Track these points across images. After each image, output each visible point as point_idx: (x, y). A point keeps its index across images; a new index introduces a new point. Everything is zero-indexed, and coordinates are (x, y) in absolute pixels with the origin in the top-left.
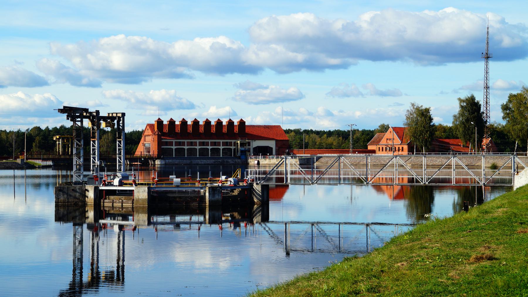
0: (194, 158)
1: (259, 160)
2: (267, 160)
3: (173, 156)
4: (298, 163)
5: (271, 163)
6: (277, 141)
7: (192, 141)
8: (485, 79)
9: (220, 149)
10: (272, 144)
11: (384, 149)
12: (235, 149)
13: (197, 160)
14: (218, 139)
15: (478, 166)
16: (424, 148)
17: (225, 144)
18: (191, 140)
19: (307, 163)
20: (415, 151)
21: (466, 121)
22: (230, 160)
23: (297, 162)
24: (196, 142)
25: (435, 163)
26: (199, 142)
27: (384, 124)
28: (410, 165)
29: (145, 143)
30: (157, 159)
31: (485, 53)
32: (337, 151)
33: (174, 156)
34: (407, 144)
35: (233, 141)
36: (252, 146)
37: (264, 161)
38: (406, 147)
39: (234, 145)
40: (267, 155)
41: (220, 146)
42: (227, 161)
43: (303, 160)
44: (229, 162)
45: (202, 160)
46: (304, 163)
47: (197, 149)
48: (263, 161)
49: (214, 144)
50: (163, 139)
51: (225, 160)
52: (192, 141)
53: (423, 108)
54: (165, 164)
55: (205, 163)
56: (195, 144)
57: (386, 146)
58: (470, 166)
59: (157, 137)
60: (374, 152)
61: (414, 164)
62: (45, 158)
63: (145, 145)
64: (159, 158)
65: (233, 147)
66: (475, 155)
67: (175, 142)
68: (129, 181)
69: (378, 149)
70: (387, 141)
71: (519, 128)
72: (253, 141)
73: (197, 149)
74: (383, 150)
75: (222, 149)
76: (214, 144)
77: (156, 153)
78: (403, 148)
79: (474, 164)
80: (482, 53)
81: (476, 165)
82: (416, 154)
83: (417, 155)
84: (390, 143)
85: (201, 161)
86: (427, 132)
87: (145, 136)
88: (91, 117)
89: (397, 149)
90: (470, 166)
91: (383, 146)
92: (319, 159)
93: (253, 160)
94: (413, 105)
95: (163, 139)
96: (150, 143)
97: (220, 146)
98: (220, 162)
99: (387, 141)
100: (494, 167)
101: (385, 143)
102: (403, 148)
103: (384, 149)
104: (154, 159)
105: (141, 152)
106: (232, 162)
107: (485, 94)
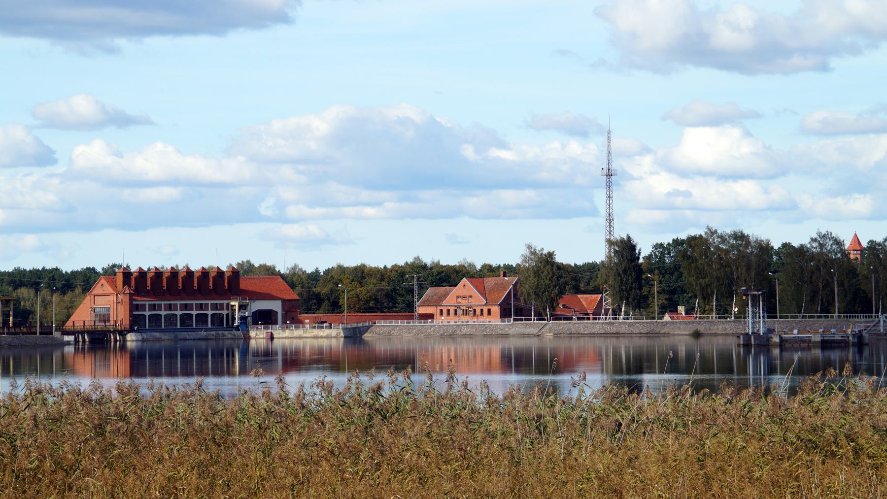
0: (184, 330)
1: (272, 331)
2: (287, 331)
3: (145, 327)
4: (342, 334)
5: (294, 335)
6: (284, 302)
7: (171, 302)
8: (608, 206)
9: (207, 315)
10: (276, 306)
11: (452, 312)
12: (227, 315)
13: (183, 333)
14: (206, 299)
15: (665, 333)
16: (548, 310)
17: (153, 307)
18: (170, 300)
19: (354, 335)
20: (533, 314)
21: (623, 272)
22: (227, 332)
23: (340, 333)
24: (176, 305)
25: (593, 331)
26: (180, 304)
27: (274, 267)
28: (551, 334)
29: (95, 306)
30: (129, 332)
31: (605, 169)
32: (402, 316)
33: (147, 327)
34: (500, 305)
35: (225, 302)
36: (251, 310)
37: (282, 332)
38: (496, 309)
39: (228, 309)
40: (259, 324)
41: (208, 310)
42: (222, 334)
43: (348, 330)
44: (226, 336)
45: (189, 333)
46: (349, 335)
47: (177, 315)
48: (279, 334)
49: (200, 307)
50: (135, 300)
51: (220, 332)
52: (171, 302)
53: (545, 252)
54: (143, 340)
55: (194, 338)
56: (143, 307)
57: (456, 308)
58: (652, 334)
59: (128, 298)
60: (431, 316)
61: (557, 333)
62: (12, 333)
63: (95, 310)
64: (131, 330)
65: (225, 312)
66: (589, 321)
67: (149, 304)
68: (607, 346)
69: (439, 312)
70: (457, 300)
71: (707, 282)
72: (252, 301)
73: (177, 315)
74: (482, 314)
75: (180, 315)
76: (200, 307)
77: (127, 323)
78: (489, 310)
79: (657, 331)
80: (603, 169)
81: (662, 332)
82: (781, 317)
83: (579, 321)
84: (464, 302)
85: (189, 335)
86: (555, 286)
87: (94, 296)
88: (744, 287)
89: (478, 312)
90: (652, 334)
91: (450, 308)
92: (369, 328)
93: (262, 332)
94: (529, 247)
95: (135, 300)
96: (109, 306)
97: (208, 310)
98: (213, 335)
99: (457, 300)
100: (697, 335)
101: (453, 303)
102: (489, 310)
103: (452, 312)
104: (123, 333)
105: (84, 322)
106: (229, 336)
107: (608, 229)
